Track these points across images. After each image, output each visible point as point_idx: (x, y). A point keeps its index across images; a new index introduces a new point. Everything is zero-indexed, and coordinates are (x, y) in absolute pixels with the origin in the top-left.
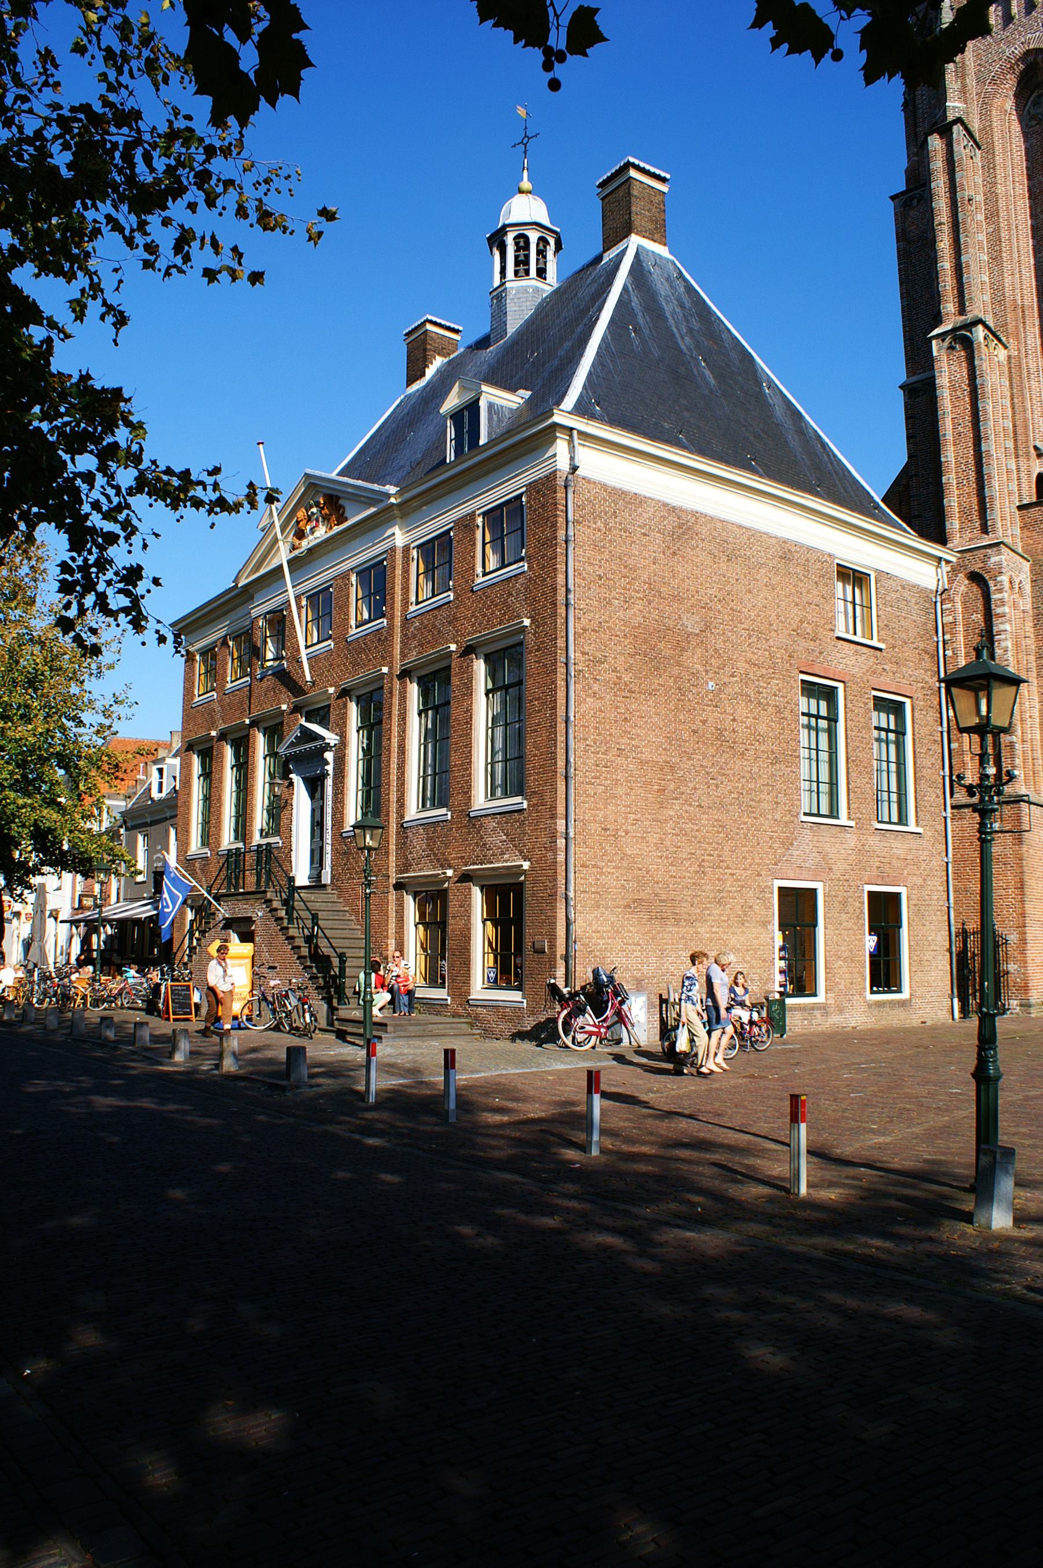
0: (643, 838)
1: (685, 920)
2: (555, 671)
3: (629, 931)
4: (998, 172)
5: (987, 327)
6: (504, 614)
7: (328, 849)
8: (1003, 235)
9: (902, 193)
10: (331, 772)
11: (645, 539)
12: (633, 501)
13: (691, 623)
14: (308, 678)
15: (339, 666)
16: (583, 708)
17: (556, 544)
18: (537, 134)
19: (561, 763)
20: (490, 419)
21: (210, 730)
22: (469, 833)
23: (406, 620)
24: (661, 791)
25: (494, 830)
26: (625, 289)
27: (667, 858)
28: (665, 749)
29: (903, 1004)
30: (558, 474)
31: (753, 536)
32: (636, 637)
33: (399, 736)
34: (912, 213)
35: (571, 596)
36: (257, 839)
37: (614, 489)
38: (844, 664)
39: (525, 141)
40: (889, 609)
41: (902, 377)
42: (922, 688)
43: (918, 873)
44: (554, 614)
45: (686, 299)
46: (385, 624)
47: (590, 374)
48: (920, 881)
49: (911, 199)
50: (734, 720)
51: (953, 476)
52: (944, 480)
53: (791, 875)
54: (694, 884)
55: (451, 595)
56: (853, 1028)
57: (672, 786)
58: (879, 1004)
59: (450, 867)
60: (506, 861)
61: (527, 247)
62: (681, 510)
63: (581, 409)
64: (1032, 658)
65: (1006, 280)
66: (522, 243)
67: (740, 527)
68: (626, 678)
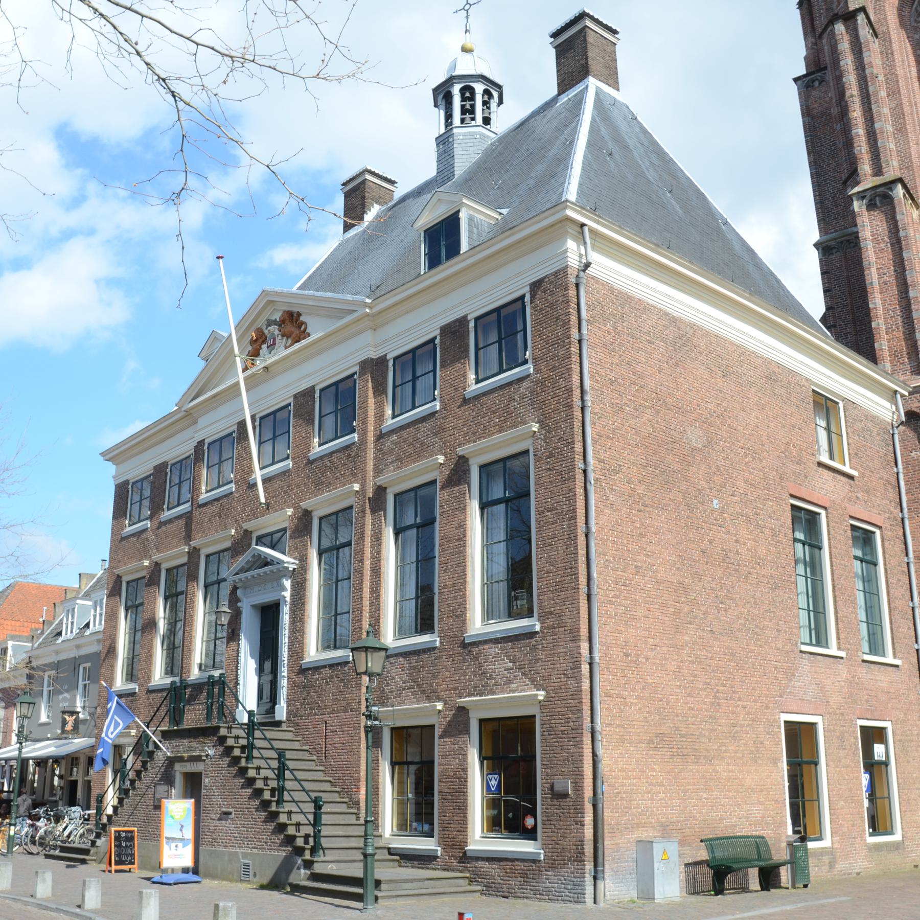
0: (662, 665)
1: (705, 757)
2: (573, 478)
3: (653, 770)
4: (896, 57)
6: (505, 421)
7: (284, 683)
8: (905, 110)
9: (804, 76)
10: (288, 599)
12: (641, 308)
13: (695, 437)
14: (263, 500)
15: (298, 486)
16: (603, 519)
17: (570, 343)
18: (478, 2)
19: (583, 579)
20: (470, 232)
21: (142, 559)
22: (464, 661)
23: (380, 437)
24: (677, 613)
25: (497, 656)
26: (593, 120)
27: (685, 687)
28: (678, 569)
29: (896, 846)
30: (570, 271)
31: (744, 354)
32: (647, 447)
33: (373, 557)
34: (814, 93)
35: (588, 398)
36: (195, 674)
37: (620, 292)
38: (823, 490)
39: (468, 6)
40: (857, 438)
41: (816, 236)
42: (889, 518)
43: (899, 707)
44: (570, 417)
45: (642, 136)
46: (356, 439)
48: (902, 716)
50: (737, 541)
51: (881, 321)
52: (874, 325)
53: (795, 709)
54: (711, 717)
55: (437, 405)
56: (858, 874)
57: (686, 609)
58: (878, 847)
59: (439, 699)
60: (514, 691)
61: (472, 98)
62: (681, 320)
65: (912, 149)
66: (468, 93)
67: (732, 343)
68: (640, 490)
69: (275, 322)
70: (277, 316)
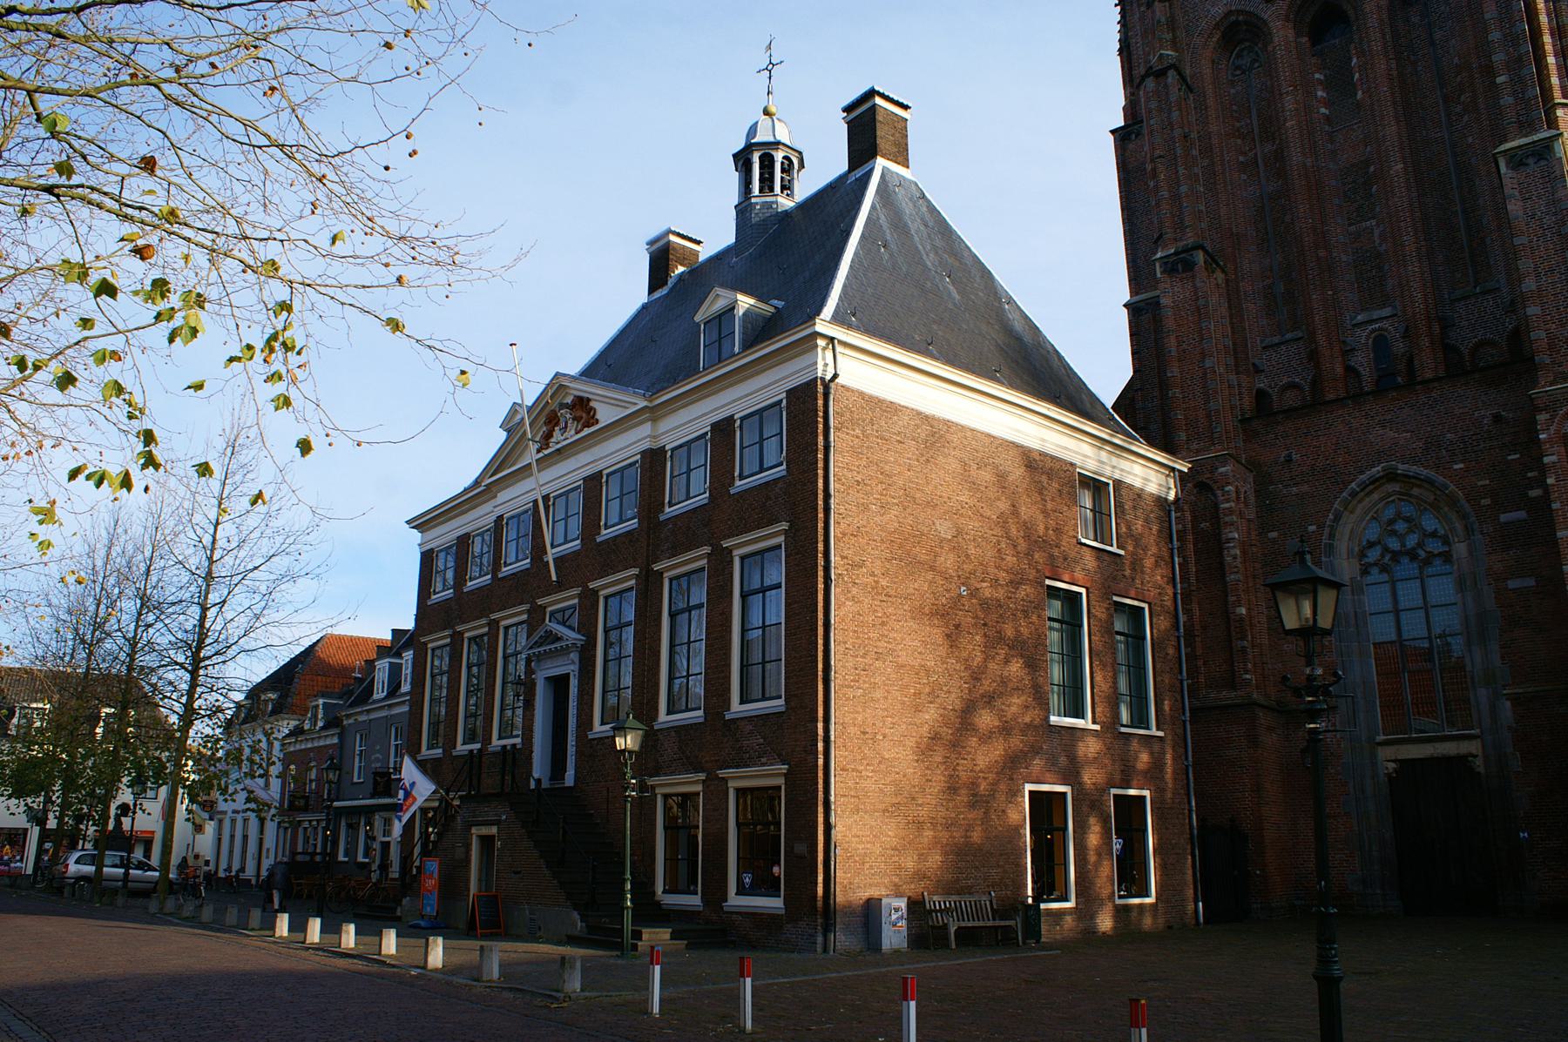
5: (1206, 251)
11: (899, 446)
12: (890, 409)
25: (751, 732)
26: (873, 207)
37: (871, 397)
41: (1126, 296)
45: (927, 217)
47: (845, 286)
49: (1130, 134)
62: (933, 418)
63: (838, 319)
64: (1258, 566)
66: (767, 162)
67: (989, 436)
69: (566, 406)
70: (569, 400)
